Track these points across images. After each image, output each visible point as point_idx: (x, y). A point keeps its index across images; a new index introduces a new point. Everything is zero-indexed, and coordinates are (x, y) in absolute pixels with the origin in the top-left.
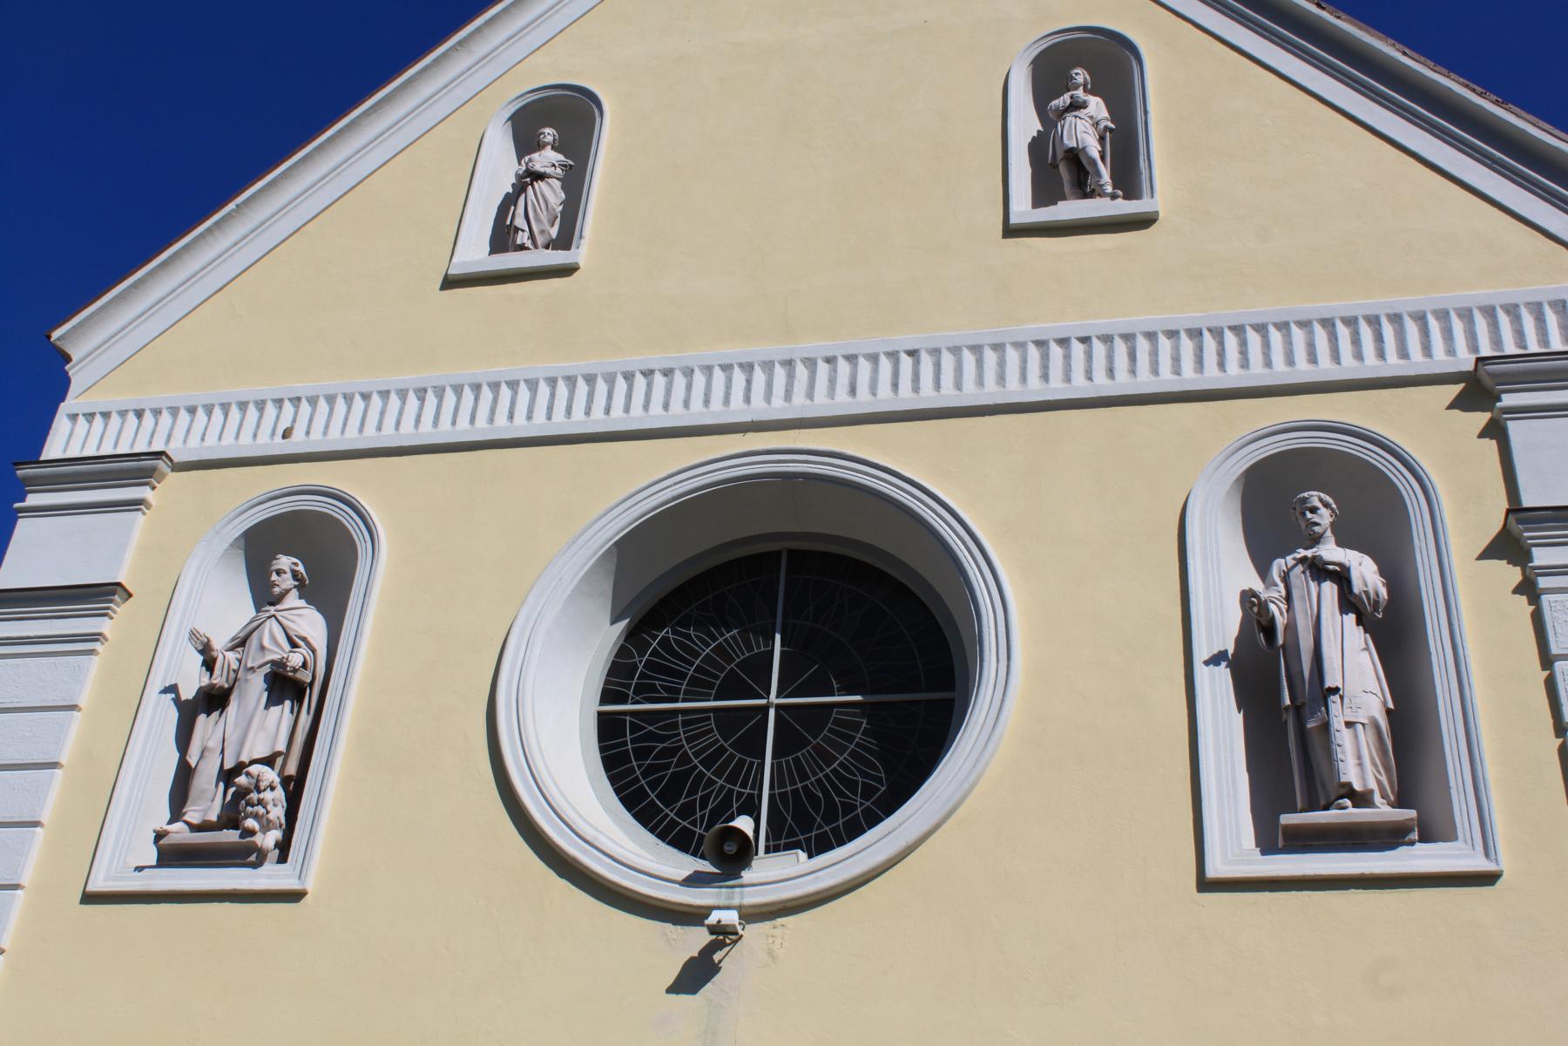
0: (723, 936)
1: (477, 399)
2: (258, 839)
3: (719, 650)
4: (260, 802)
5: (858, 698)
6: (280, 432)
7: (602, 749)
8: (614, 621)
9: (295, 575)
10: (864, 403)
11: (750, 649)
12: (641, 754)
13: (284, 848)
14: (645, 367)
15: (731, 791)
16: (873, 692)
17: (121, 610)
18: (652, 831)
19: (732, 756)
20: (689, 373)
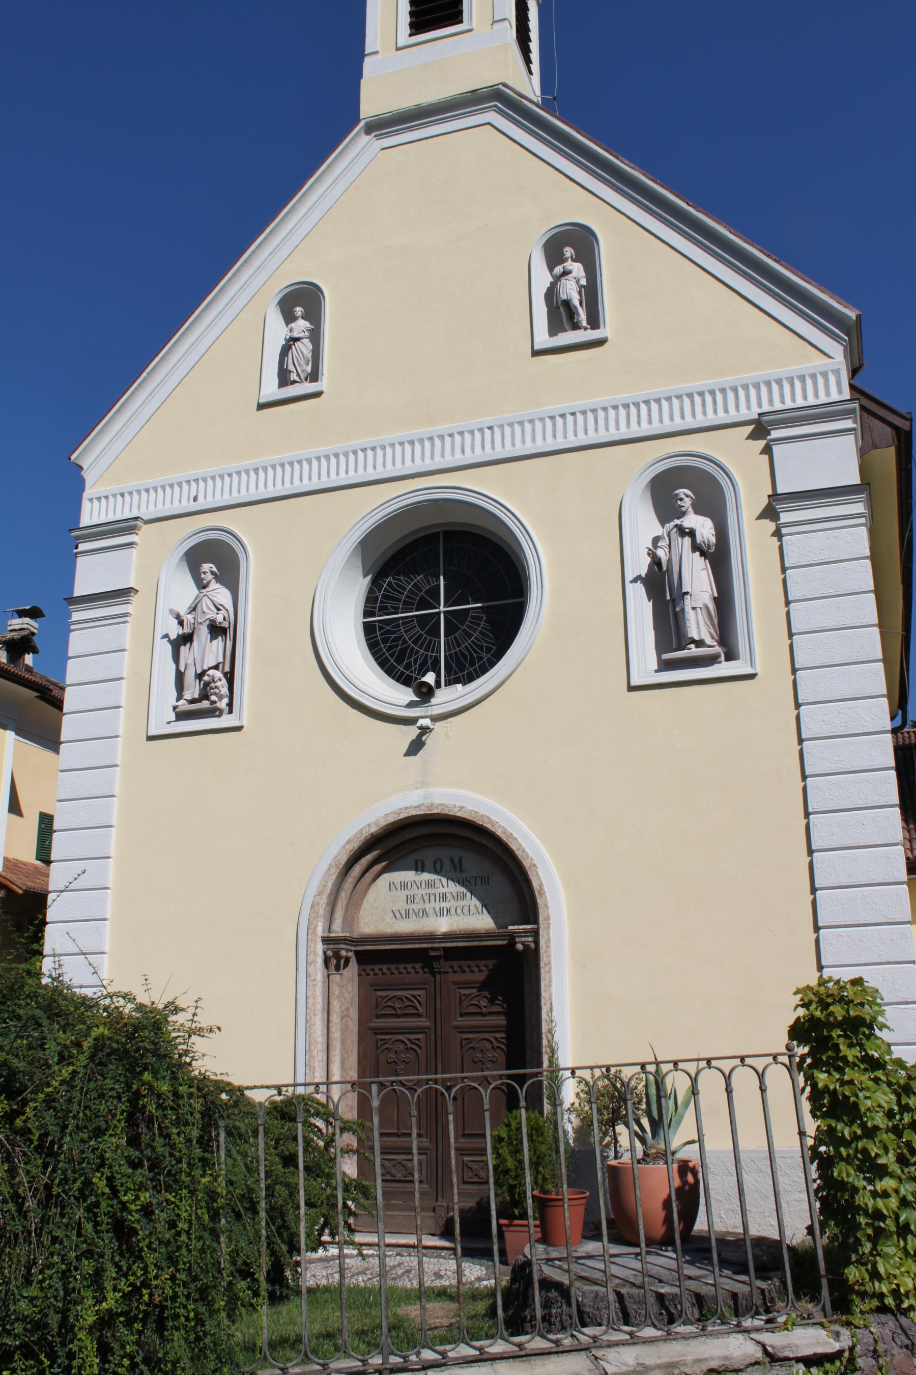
0: (425, 730)
1: (283, 471)
2: (218, 705)
3: (415, 586)
4: (216, 687)
5: (480, 605)
6: (192, 499)
7: (367, 640)
8: (365, 576)
9: (212, 573)
10: (469, 458)
11: (429, 584)
12: (385, 641)
13: (230, 705)
14: (362, 447)
15: (427, 655)
16: (488, 601)
17: (135, 599)
18: (393, 678)
19: (426, 638)
20: (383, 448)
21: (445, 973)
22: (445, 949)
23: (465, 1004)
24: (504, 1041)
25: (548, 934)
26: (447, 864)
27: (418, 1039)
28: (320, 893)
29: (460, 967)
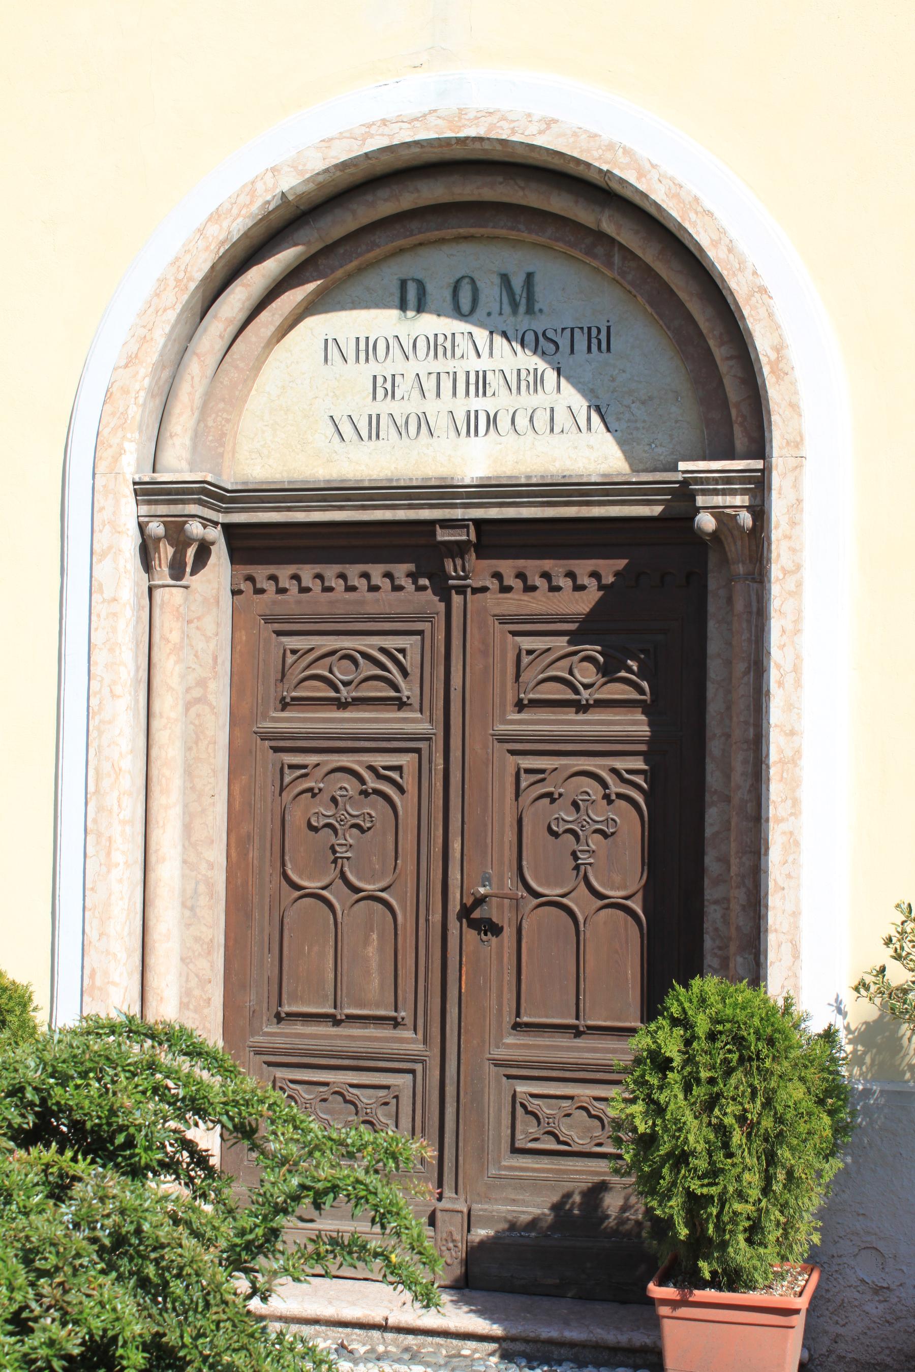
21: (475, 591)
22: (479, 523)
23: (529, 676)
24: (639, 780)
25: (796, 485)
26: (491, 292)
27: (399, 769)
28: (131, 361)
29: (521, 576)
